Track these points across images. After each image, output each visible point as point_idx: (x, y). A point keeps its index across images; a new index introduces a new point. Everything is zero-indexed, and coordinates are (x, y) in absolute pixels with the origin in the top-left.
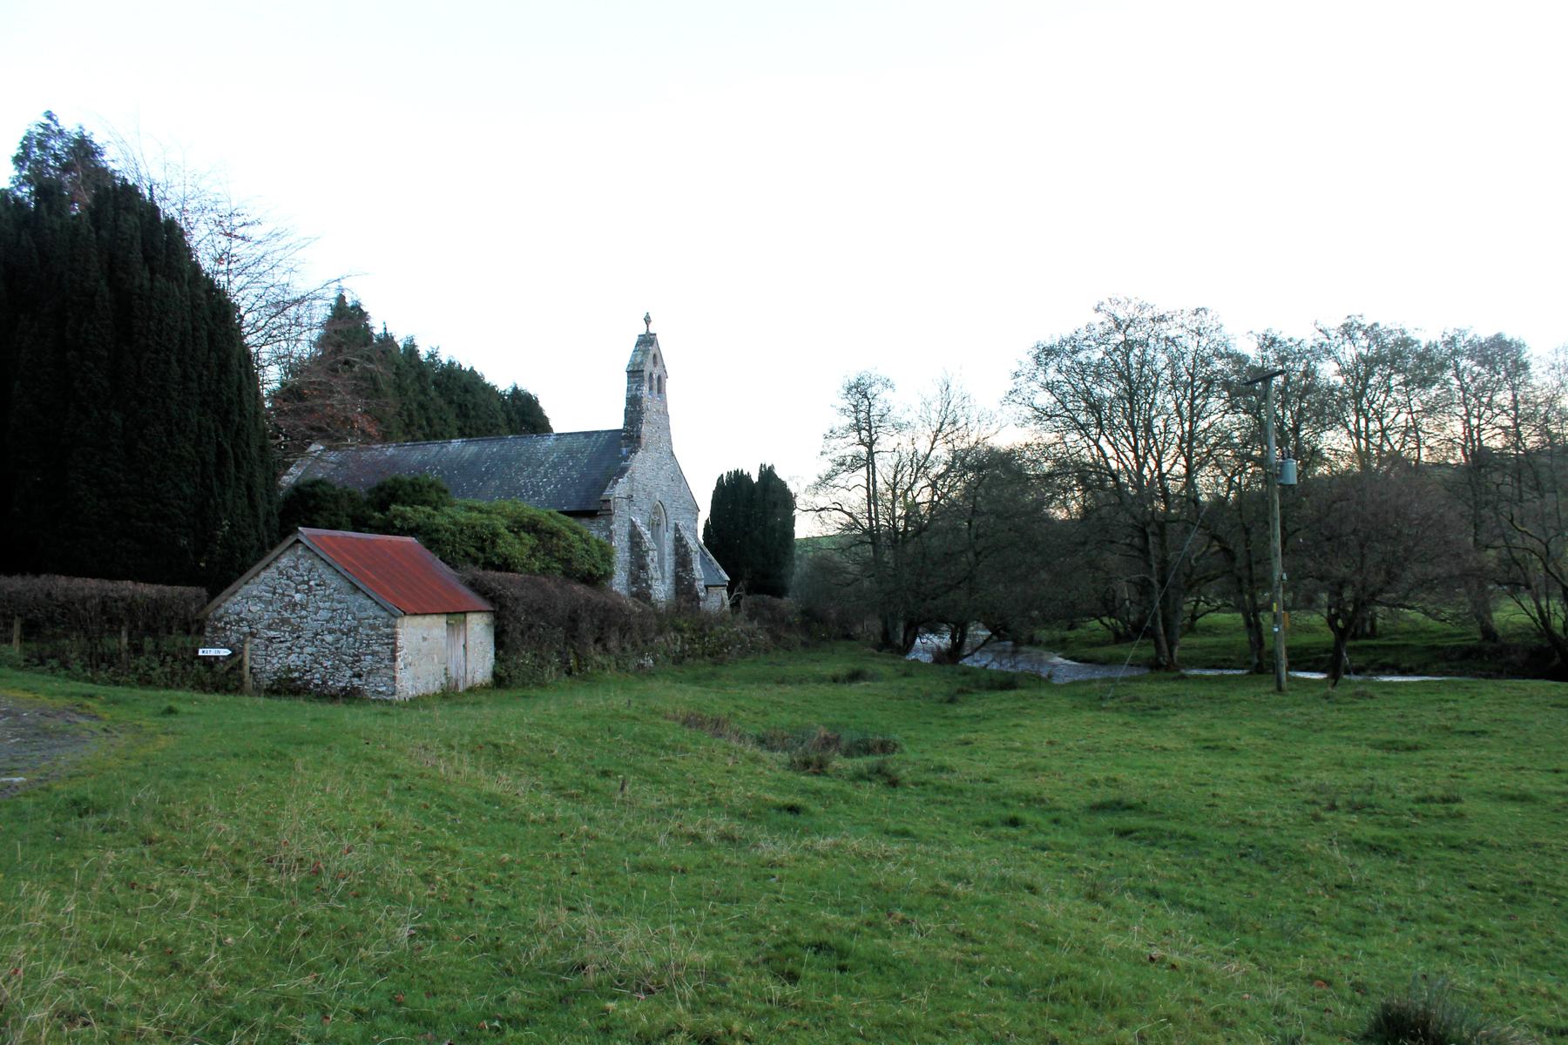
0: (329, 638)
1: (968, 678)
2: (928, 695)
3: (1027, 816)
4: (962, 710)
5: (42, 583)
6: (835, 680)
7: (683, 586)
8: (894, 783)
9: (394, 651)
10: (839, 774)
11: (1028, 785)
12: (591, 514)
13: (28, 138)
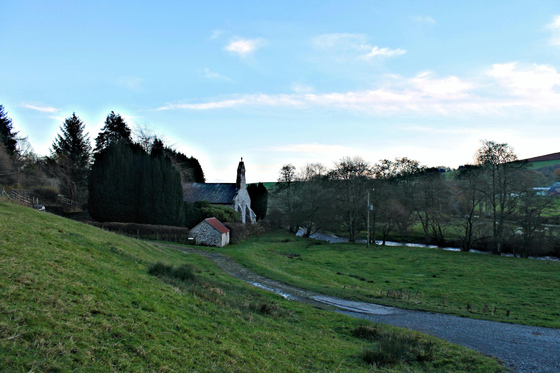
0: (210, 237)
1: (311, 242)
2: (303, 246)
3: (318, 263)
4: (310, 249)
5: (161, 226)
6: (283, 241)
7: (248, 219)
8: (302, 260)
9: (221, 239)
10: (294, 259)
11: (318, 261)
12: (230, 204)
13: (108, 117)
